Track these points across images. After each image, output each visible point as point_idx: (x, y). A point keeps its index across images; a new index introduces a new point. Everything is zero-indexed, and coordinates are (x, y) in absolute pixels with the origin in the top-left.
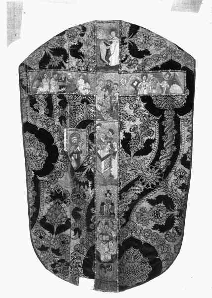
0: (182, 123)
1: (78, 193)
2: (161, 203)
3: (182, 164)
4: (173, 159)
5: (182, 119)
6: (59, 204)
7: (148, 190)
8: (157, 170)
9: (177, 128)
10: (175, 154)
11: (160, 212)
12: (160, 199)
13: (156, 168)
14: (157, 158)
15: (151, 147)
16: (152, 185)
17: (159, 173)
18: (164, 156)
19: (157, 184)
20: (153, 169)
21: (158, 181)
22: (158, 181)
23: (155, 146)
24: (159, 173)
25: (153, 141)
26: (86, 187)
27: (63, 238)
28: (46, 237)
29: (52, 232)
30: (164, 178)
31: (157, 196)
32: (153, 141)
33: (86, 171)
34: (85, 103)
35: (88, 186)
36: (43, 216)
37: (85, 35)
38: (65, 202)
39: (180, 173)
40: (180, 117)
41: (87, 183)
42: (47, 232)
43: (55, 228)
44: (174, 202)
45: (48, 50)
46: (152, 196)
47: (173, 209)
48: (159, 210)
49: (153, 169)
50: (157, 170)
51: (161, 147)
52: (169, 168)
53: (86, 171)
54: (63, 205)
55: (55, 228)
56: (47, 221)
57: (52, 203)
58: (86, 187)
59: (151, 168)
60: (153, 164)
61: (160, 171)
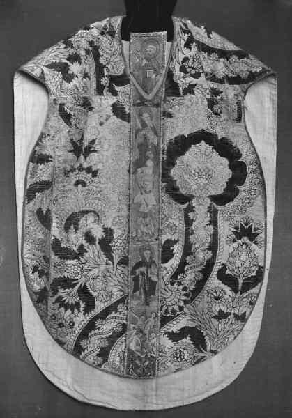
0: (219, 215)
1: (60, 321)
2: (186, 337)
3: (219, 279)
4: (104, 315)
5: (220, 211)
6: (247, 246)
7: (167, 317)
8: (181, 287)
9: (214, 222)
10: (209, 265)
11: (185, 352)
12: (184, 332)
13: (179, 284)
14: (181, 269)
15: (173, 250)
16: (174, 311)
17: (184, 292)
18: (191, 265)
19: (181, 308)
20: (175, 286)
21: (182, 304)
22: (182, 304)
23: (178, 250)
24: (184, 292)
25: (175, 242)
26: (76, 311)
27: (251, 297)
28: (226, 297)
29: (235, 290)
30: (192, 300)
31: (181, 327)
32: (175, 242)
33: (78, 286)
34: (80, 186)
35: (79, 311)
36: (223, 264)
37: (181, 60)
38: (256, 243)
39: (216, 292)
40: (219, 208)
41: (77, 305)
42: (227, 289)
43: (241, 281)
44: (206, 338)
45: (82, 281)
46: (175, 326)
47: (206, 350)
48: (184, 349)
49: (175, 286)
50: (181, 287)
51: (188, 250)
52: (200, 285)
53: (78, 286)
54: (254, 246)
55: (241, 281)
56: (228, 272)
57: (235, 245)
58: (76, 311)
59: (172, 284)
60: (175, 276)
61: (185, 289)
